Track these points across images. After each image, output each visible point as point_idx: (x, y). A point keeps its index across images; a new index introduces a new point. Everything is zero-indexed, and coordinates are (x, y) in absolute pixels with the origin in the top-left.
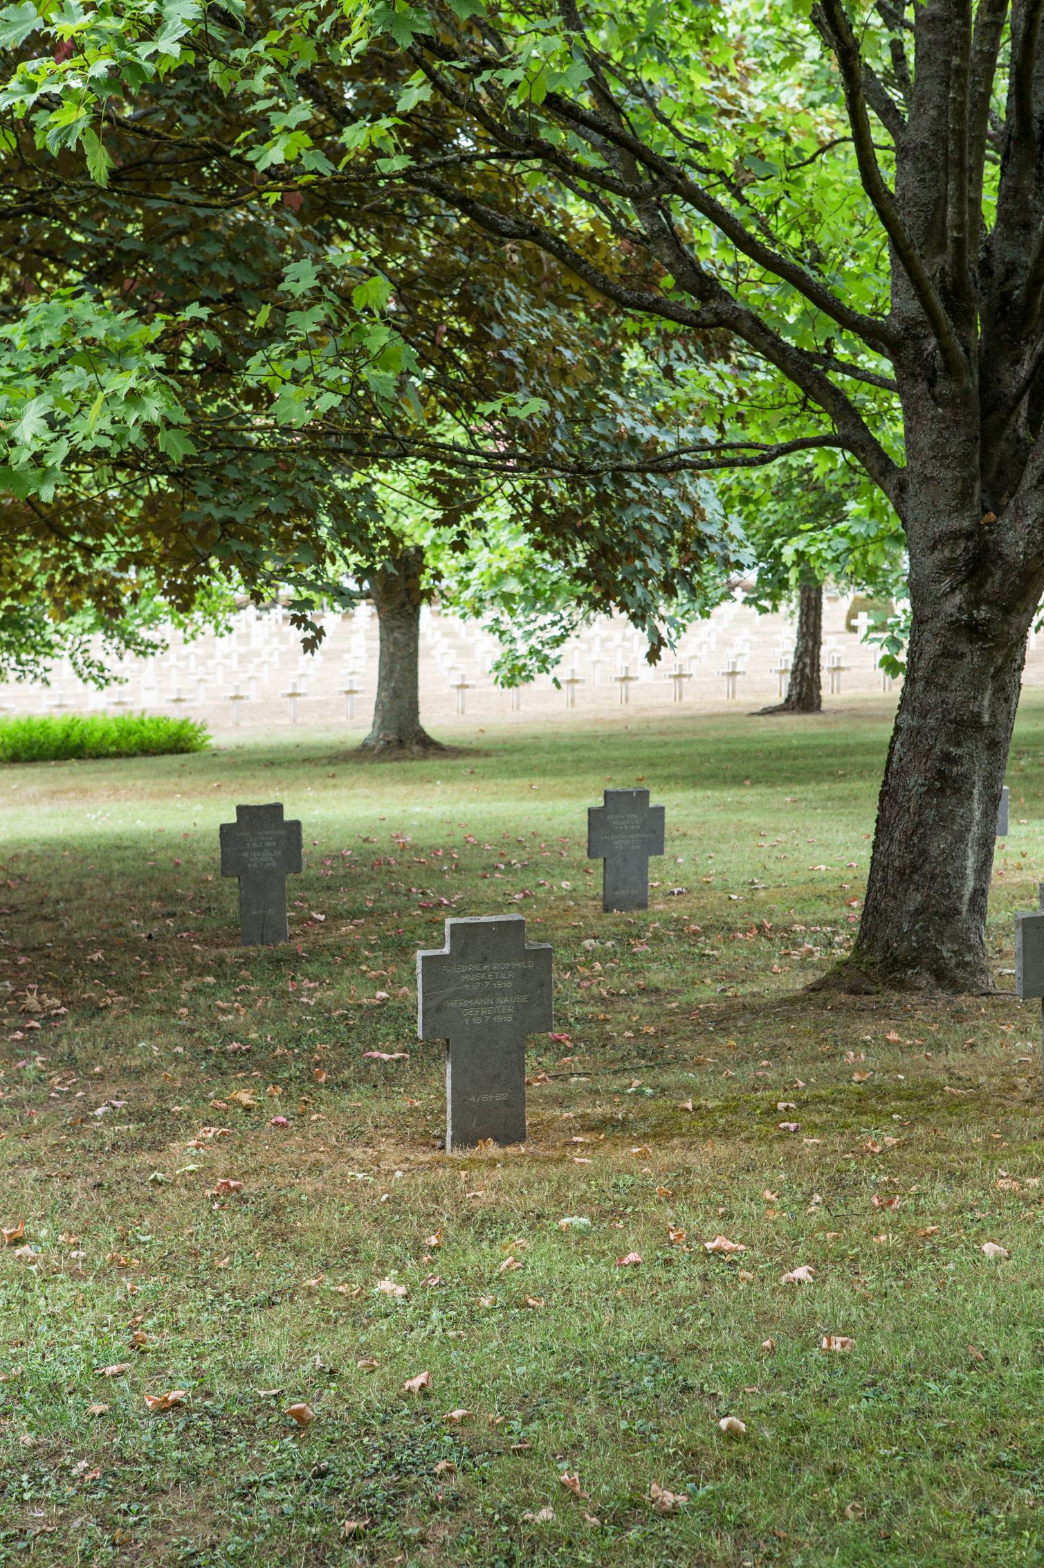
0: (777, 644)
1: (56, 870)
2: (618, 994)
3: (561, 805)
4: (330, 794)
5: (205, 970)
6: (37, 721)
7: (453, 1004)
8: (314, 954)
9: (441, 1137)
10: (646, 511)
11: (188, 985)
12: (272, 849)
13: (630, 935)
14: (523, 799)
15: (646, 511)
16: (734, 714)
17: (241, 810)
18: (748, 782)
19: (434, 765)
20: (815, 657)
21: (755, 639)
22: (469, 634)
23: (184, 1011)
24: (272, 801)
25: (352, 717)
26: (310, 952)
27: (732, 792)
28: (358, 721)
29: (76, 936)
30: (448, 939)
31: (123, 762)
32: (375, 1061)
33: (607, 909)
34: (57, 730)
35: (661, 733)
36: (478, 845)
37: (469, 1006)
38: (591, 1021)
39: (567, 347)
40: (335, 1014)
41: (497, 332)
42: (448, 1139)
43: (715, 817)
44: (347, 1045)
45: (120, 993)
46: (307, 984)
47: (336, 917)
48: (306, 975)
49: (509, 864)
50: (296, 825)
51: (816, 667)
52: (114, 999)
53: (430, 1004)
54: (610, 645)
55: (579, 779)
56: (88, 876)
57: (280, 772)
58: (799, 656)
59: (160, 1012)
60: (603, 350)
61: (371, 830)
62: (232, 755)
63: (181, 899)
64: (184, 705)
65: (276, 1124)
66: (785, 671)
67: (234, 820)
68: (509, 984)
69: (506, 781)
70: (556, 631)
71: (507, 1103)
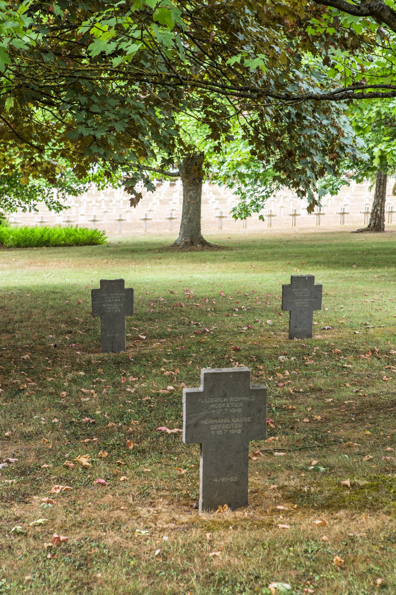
0: (363, 201)
1: (21, 304)
2: (299, 392)
3: (266, 276)
4: (157, 267)
5: (80, 367)
6: (29, 228)
7: (205, 422)
8: (137, 359)
9: (196, 500)
10: (314, 132)
11: (70, 376)
12: (118, 303)
13: (304, 354)
14: (248, 272)
15: (314, 132)
16: (344, 232)
17: (102, 282)
18: (354, 266)
19: (207, 254)
20: (382, 207)
21: (352, 198)
22: (225, 194)
23: (64, 393)
24: (118, 278)
25: (171, 230)
26: (135, 358)
27: (348, 271)
28: (173, 233)
29: (19, 343)
30: (202, 382)
31: (66, 249)
32: (163, 433)
33: (291, 337)
34: (38, 234)
35: (311, 241)
36: (225, 297)
37: (215, 424)
38: (284, 410)
39: (277, 45)
40: (145, 399)
41: (241, 37)
42: (200, 504)
43: (341, 285)
44: (149, 422)
45: (33, 381)
46: (131, 379)
47: (152, 337)
48: (132, 372)
49: (240, 309)
50: (131, 290)
51: (382, 211)
52: (28, 385)
53: (190, 422)
54: (287, 200)
55: (274, 262)
56: (36, 308)
57: (136, 256)
58: (375, 206)
59: (51, 394)
60: (292, 54)
61: (175, 287)
62: (116, 246)
63: (76, 323)
64: (97, 223)
65: (99, 483)
66: (367, 213)
67: (99, 287)
68: (240, 410)
69: (240, 263)
70: (264, 194)
71: (237, 483)
